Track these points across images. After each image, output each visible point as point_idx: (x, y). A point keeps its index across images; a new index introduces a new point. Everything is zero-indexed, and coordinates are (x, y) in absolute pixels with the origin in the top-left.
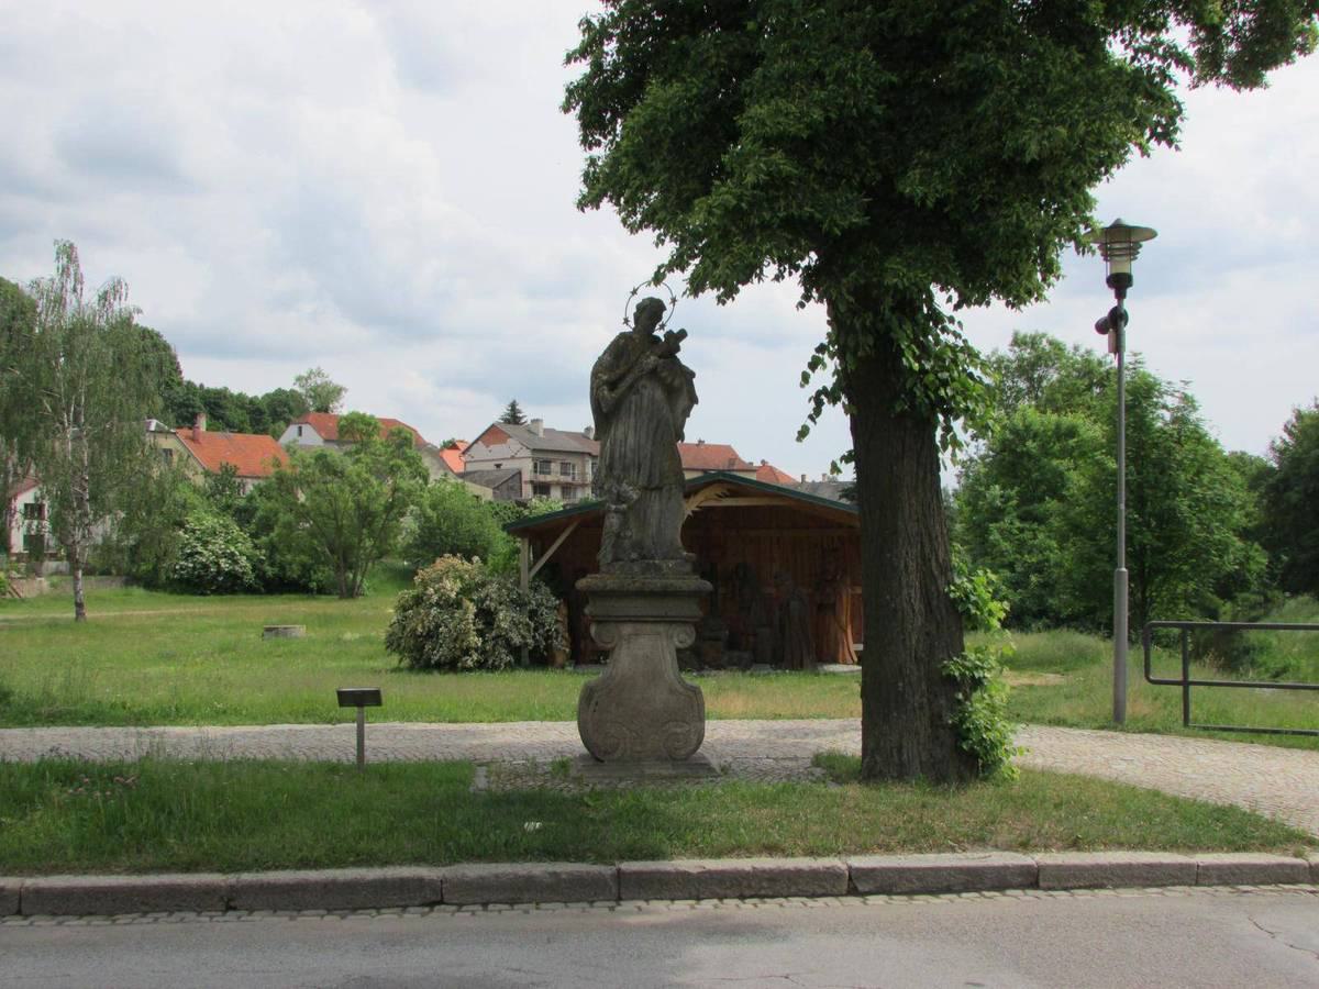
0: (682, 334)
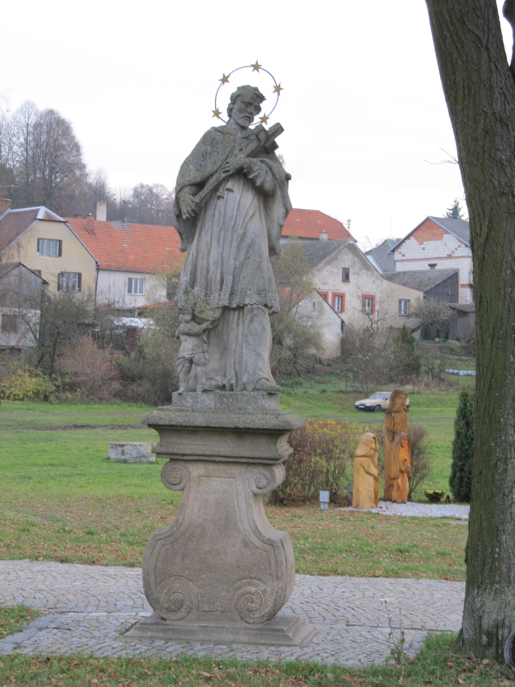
0: (278, 129)
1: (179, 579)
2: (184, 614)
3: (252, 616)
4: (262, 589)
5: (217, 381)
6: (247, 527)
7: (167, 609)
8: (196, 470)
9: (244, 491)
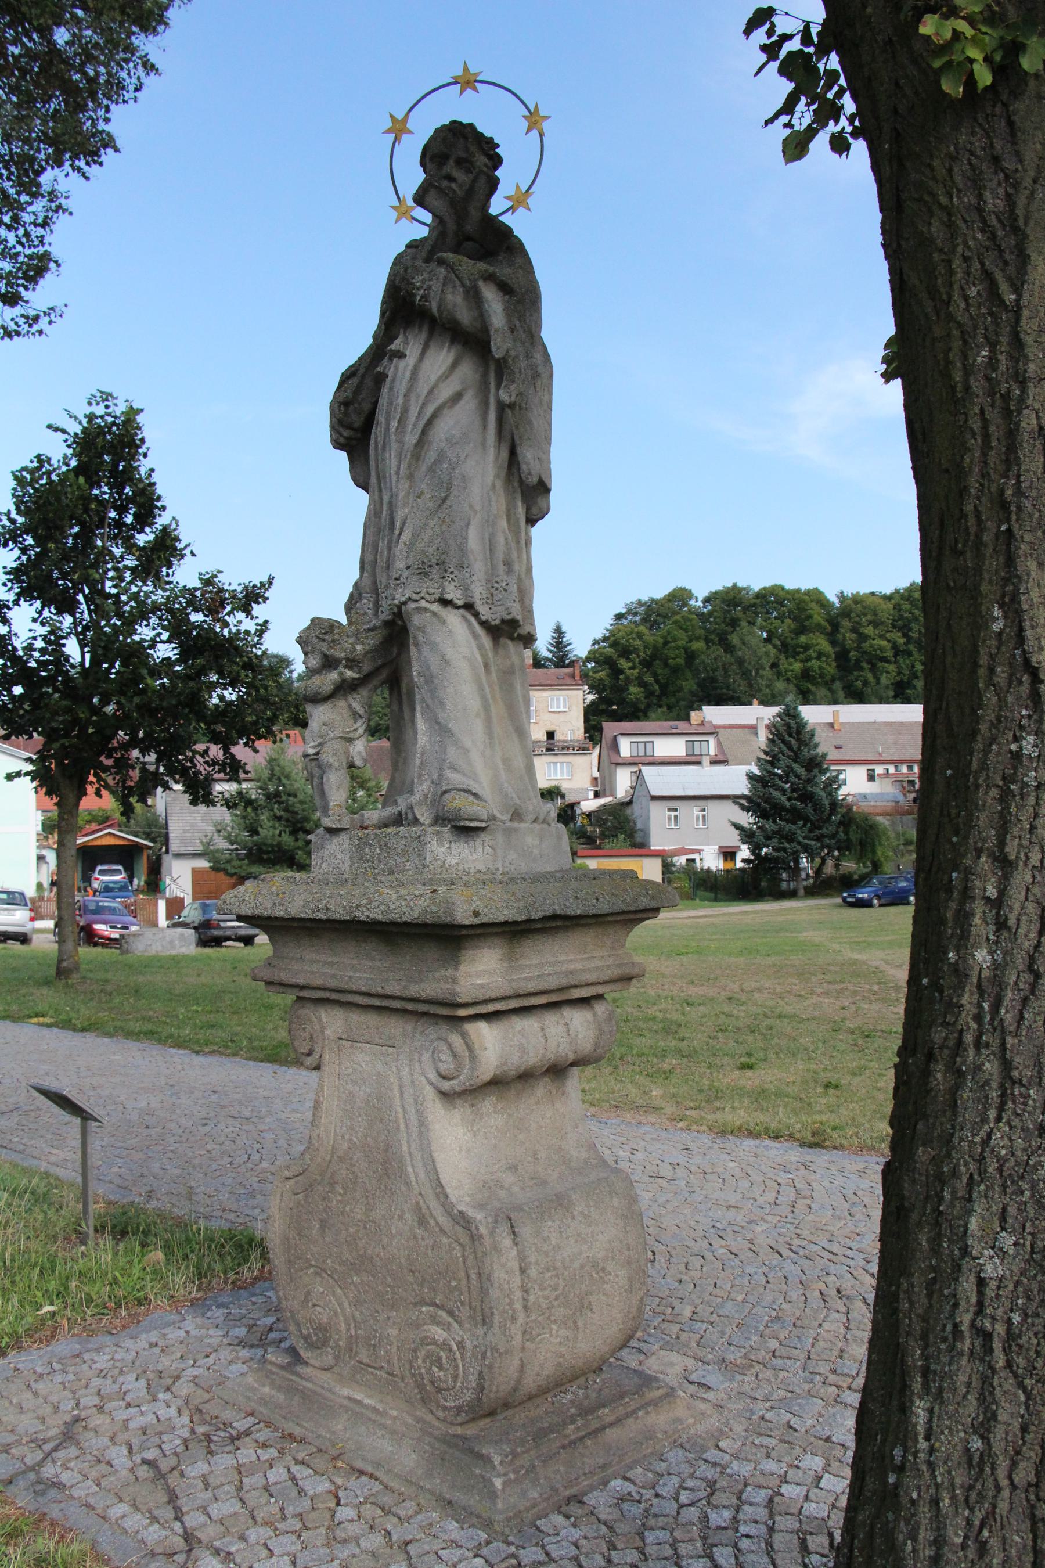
3: (442, 1402)
4: (458, 1338)
8: (332, 1022)
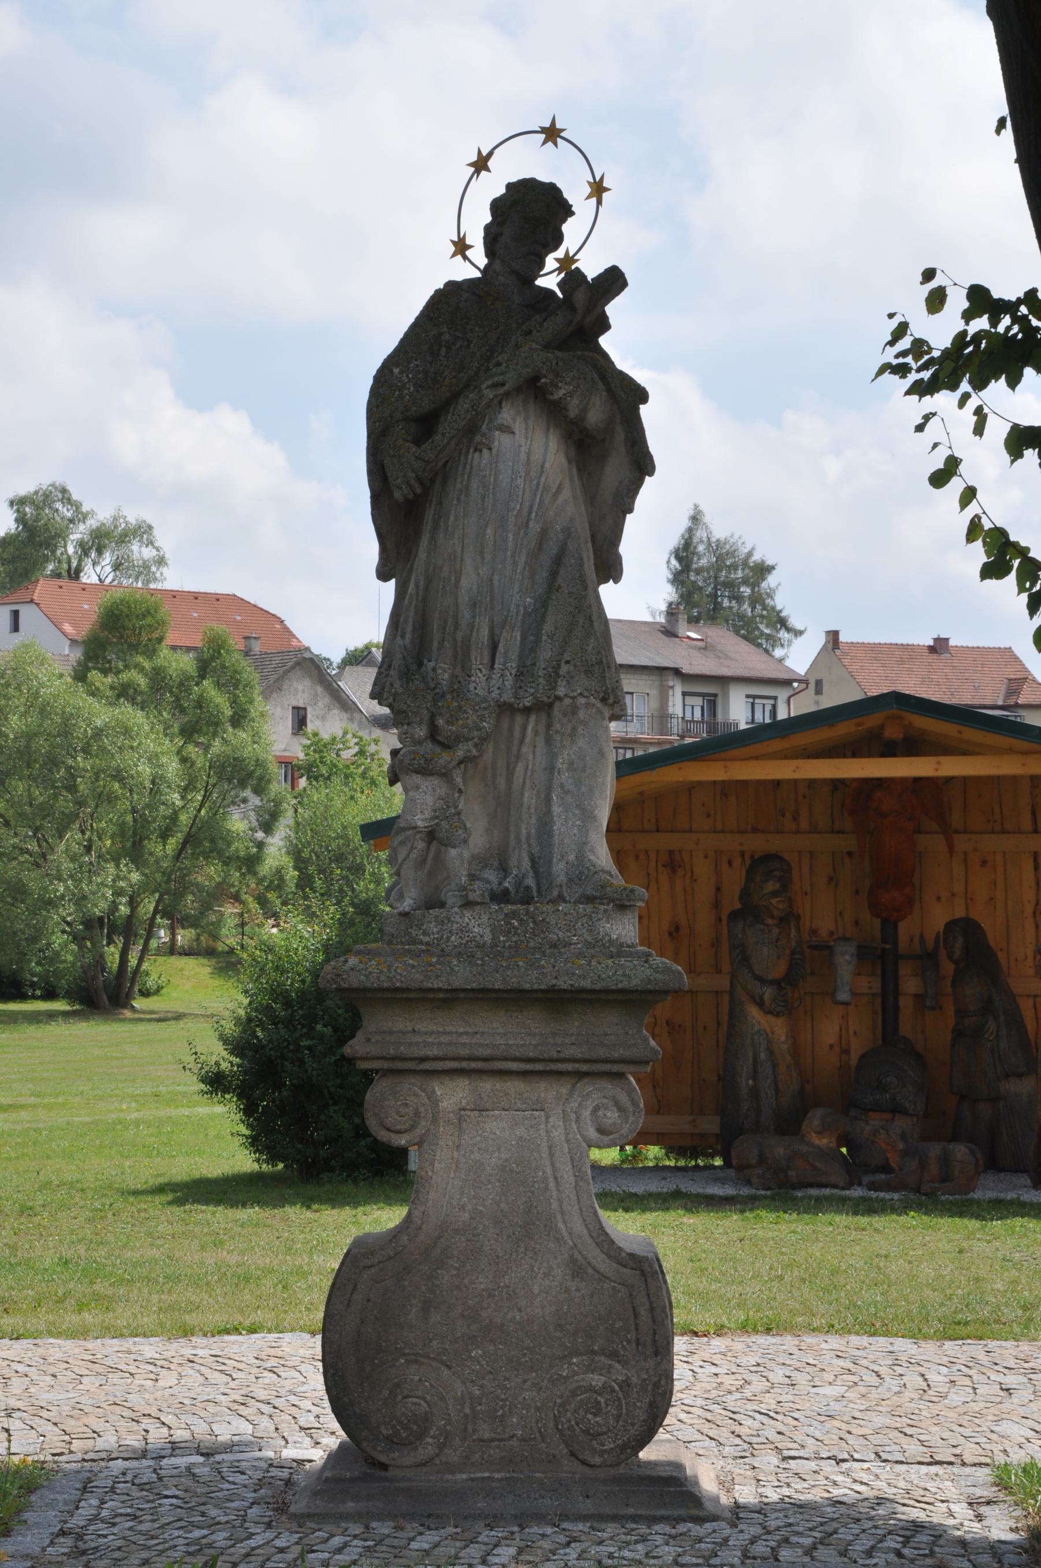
0: (613, 281)
1: (416, 1362)
2: (431, 1450)
5: (488, 882)
6: (579, 1227)
7: (389, 1439)
9: (568, 1141)
